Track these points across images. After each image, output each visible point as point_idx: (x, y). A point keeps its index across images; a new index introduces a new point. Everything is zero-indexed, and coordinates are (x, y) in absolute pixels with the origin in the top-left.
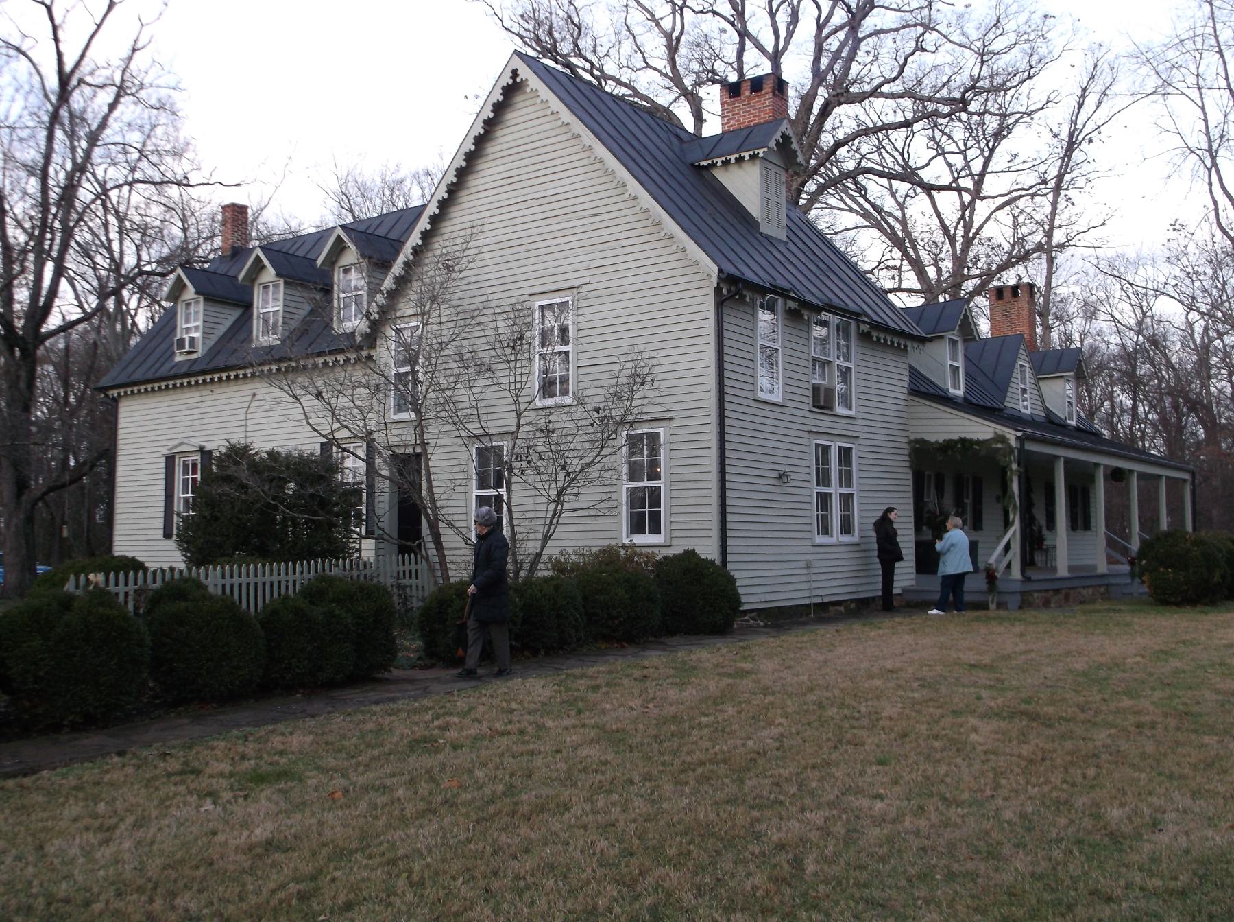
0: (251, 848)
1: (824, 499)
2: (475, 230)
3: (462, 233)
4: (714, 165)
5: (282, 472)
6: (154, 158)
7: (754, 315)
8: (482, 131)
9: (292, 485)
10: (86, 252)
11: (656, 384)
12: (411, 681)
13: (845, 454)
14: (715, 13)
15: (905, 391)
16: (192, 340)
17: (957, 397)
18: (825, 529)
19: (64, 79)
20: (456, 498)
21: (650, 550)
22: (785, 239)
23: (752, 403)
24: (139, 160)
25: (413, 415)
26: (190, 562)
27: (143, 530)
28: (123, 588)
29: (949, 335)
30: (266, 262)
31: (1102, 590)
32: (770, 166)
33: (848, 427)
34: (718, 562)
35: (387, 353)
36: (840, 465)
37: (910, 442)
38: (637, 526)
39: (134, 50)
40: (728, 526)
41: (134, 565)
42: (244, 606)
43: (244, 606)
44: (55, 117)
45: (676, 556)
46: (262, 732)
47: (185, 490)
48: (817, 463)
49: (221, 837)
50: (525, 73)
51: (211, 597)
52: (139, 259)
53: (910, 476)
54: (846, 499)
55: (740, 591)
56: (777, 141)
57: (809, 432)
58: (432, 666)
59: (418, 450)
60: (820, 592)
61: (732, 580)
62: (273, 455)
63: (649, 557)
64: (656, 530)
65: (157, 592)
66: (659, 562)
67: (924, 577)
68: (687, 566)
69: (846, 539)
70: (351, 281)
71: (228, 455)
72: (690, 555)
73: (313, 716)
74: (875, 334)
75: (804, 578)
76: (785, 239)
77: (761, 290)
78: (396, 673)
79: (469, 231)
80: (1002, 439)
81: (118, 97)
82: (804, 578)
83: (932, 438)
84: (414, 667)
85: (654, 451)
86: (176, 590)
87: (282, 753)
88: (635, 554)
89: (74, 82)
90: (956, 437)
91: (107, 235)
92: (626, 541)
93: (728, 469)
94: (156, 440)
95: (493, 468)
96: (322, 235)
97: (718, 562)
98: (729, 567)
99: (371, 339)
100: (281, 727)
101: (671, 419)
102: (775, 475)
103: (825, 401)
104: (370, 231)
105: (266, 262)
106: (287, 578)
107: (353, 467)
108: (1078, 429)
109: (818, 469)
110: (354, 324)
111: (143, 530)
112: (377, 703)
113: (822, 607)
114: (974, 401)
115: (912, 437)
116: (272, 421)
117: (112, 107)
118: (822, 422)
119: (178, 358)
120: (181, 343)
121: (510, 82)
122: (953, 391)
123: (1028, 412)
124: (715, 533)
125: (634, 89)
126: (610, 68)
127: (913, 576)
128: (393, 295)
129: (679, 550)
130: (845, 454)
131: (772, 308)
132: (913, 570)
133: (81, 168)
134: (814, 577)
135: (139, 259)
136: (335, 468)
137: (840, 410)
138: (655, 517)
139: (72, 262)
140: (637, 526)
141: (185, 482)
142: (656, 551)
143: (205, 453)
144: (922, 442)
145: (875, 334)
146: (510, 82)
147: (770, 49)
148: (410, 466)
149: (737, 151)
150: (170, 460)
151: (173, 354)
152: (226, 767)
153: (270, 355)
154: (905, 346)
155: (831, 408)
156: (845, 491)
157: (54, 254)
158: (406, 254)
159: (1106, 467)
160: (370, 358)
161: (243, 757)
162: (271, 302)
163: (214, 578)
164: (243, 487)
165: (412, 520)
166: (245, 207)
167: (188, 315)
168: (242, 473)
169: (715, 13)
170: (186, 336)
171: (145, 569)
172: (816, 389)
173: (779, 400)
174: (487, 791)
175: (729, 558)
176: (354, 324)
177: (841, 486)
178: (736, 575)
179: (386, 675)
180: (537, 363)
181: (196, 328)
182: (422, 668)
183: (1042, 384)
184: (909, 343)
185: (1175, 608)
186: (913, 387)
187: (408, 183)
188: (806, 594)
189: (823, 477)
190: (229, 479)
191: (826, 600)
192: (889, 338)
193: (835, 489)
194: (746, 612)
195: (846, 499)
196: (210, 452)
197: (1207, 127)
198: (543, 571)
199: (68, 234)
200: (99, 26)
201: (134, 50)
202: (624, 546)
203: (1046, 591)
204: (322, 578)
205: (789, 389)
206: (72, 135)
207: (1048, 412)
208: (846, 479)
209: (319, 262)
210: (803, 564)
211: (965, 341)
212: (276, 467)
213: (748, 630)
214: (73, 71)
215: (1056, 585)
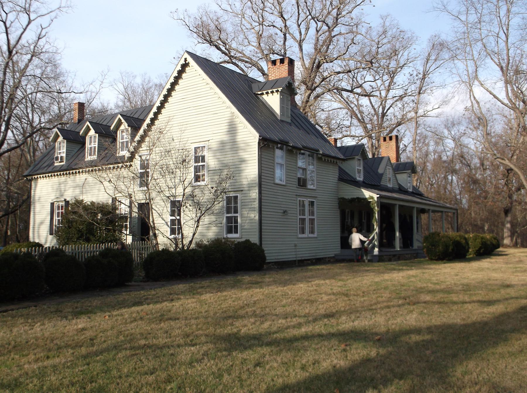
0: (77, 330)
1: (303, 221)
2: (171, 118)
3: (166, 119)
4: (262, 94)
5: (95, 210)
6: (46, 80)
7: (274, 152)
8: (173, 81)
9: (99, 215)
10: (19, 119)
11: (235, 178)
12: (139, 286)
13: (312, 204)
14: (274, 26)
15: (337, 179)
16: (62, 157)
17: (360, 181)
18: (303, 231)
19: (10, 52)
20: (161, 219)
21: (233, 240)
22: (290, 121)
23: (273, 185)
24: (40, 81)
25: (146, 188)
26: (59, 244)
27: (42, 232)
28: (35, 252)
29: (357, 157)
30: (91, 127)
31: (415, 255)
32: (284, 94)
33: (313, 193)
34: (258, 244)
35: (137, 162)
36: (309, 207)
37: (339, 199)
38: (230, 230)
39: (39, 38)
40: (263, 231)
41: (39, 245)
42: (80, 259)
43: (80, 259)
44: (7, 66)
45: (242, 242)
46: (83, 301)
47: (58, 217)
48: (300, 207)
49: (68, 327)
50: (190, 60)
51: (67, 255)
52: (40, 120)
53: (339, 212)
54: (312, 221)
55: (266, 255)
56: (286, 85)
57: (296, 195)
58: (148, 281)
59: (148, 201)
60: (301, 256)
61: (263, 251)
62: (93, 203)
63: (233, 242)
64: (236, 232)
65: (47, 253)
66: (236, 244)
67: (343, 250)
68: (246, 246)
69: (311, 235)
70: (124, 133)
71: (75, 204)
72: (248, 241)
73: (102, 296)
74: (323, 158)
75: (294, 250)
76: (290, 121)
77: (277, 143)
78: (133, 283)
79: (168, 118)
80: (372, 198)
81: (32, 56)
82: (294, 250)
83: (346, 197)
84: (141, 282)
85: (236, 202)
86: (53, 253)
87: (90, 306)
88: (227, 241)
89: (14, 52)
90: (355, 197)
91: (27, 111)
92: (225, 236)
93: (263, 209)
94: (47, 193)
95: (176, 207)
96: (114, 116)
97: (258, 244)
98: (263, 246)
99: (131, 158)
100: (90, 299)
101: (242, 191)
102: (282, 211)
103: (303, 184)
104: (131, 116)
105: (91, 127)
106: (94, 248)
107: (123, 209)
108: (412, 193)
109: (300, 210)
110: (125, 153)
111: (42, 232)
112: (125, 292)
113: (300, 261)
114: (367, 182)
115: (340, 197)
116: (94, 189)
117: (30, 60)
118: (302, 191)
119: (56, 164)
120: (57, 159)
121: (184, 63)
122: (358, 179)
123: (391, 186)
124: (257, 234)
125: (244, 54)
126: (234, 45)
127: (340, 250)
128: (140, 142)
129: (243, 240)
130: (312, 204)
131: (281, 148)
132: (340, 247)
133: (16, 87)
134: (298, 250)
135: (40, 120)
136: (115, 208)
137: (310, 187)
138: (236, 227)
139: (13, 122)
140: (230, 230)
141: (58, 213)
142: (235, 240)
143: (67, 202)
144: (343, 199)
145: (323, 158)
146: (184, 63)
147: (298, 39)
148: (145, 208)
149: (272, 88)
150: (52, 204)
151: (54, 162)
152: (70, 310)
153: (92, 164)
154: (336, 162)
155: (306, 186)
156: (311, 217)
157: (6, 119)
158: (144, 126)
159: (417, 208)
160: (131, 166)
161: (76, 308)
162: (92, 139)
163: (68, 249)
164: (81, 216)
165: (144, 229)
166: (84, 104)
167: (60, 147)
168: (81, 211)
169: (274, 26)
170: (59, 156)
171: (43, 247)
172: (299, 179)
173: (284, 183)
174: (155, 316)
175: (263, 243)
176: (125, 153)
177: (310, 215)
178: (265, 249)
179: (130, 284)
180: (192, 169)
181: (63, 152)
182: (144, 282)
183: (398, 176)
184: (338, 161)
185: (435, 261)
186: (341, 177)
187: (152, 90)
188: (295, 256)
189: (303, 213)
190: (75, 213)
191: (303, 258)
192: (326, 159)
193: (307, 217)
194: (269, 263)
195: (312, 221)
196: (68, 202)
197: (468, 73)
198: (193, 246)
199: (11, 111)
200: (25, 30)
201: (39, 38)
202: (224, 238)
203: (390, 255)
204: (108, 250)
205: (288, 179)
206: (14, 72)
207: (399, 185)
208: (312, 213)
209: (112, 128)
210: (293, 245)
211: (363, 159)
212: (94, 209)
213: (270, 269)
214: (15, 46)
215: (394, 253)
